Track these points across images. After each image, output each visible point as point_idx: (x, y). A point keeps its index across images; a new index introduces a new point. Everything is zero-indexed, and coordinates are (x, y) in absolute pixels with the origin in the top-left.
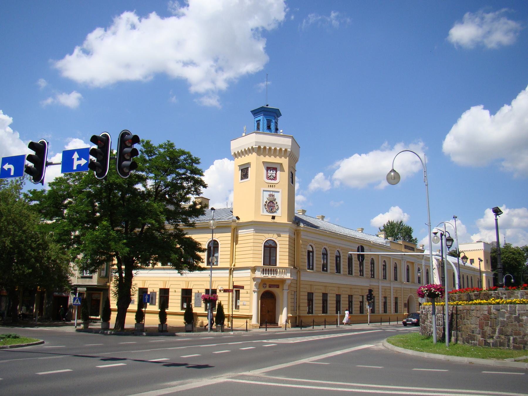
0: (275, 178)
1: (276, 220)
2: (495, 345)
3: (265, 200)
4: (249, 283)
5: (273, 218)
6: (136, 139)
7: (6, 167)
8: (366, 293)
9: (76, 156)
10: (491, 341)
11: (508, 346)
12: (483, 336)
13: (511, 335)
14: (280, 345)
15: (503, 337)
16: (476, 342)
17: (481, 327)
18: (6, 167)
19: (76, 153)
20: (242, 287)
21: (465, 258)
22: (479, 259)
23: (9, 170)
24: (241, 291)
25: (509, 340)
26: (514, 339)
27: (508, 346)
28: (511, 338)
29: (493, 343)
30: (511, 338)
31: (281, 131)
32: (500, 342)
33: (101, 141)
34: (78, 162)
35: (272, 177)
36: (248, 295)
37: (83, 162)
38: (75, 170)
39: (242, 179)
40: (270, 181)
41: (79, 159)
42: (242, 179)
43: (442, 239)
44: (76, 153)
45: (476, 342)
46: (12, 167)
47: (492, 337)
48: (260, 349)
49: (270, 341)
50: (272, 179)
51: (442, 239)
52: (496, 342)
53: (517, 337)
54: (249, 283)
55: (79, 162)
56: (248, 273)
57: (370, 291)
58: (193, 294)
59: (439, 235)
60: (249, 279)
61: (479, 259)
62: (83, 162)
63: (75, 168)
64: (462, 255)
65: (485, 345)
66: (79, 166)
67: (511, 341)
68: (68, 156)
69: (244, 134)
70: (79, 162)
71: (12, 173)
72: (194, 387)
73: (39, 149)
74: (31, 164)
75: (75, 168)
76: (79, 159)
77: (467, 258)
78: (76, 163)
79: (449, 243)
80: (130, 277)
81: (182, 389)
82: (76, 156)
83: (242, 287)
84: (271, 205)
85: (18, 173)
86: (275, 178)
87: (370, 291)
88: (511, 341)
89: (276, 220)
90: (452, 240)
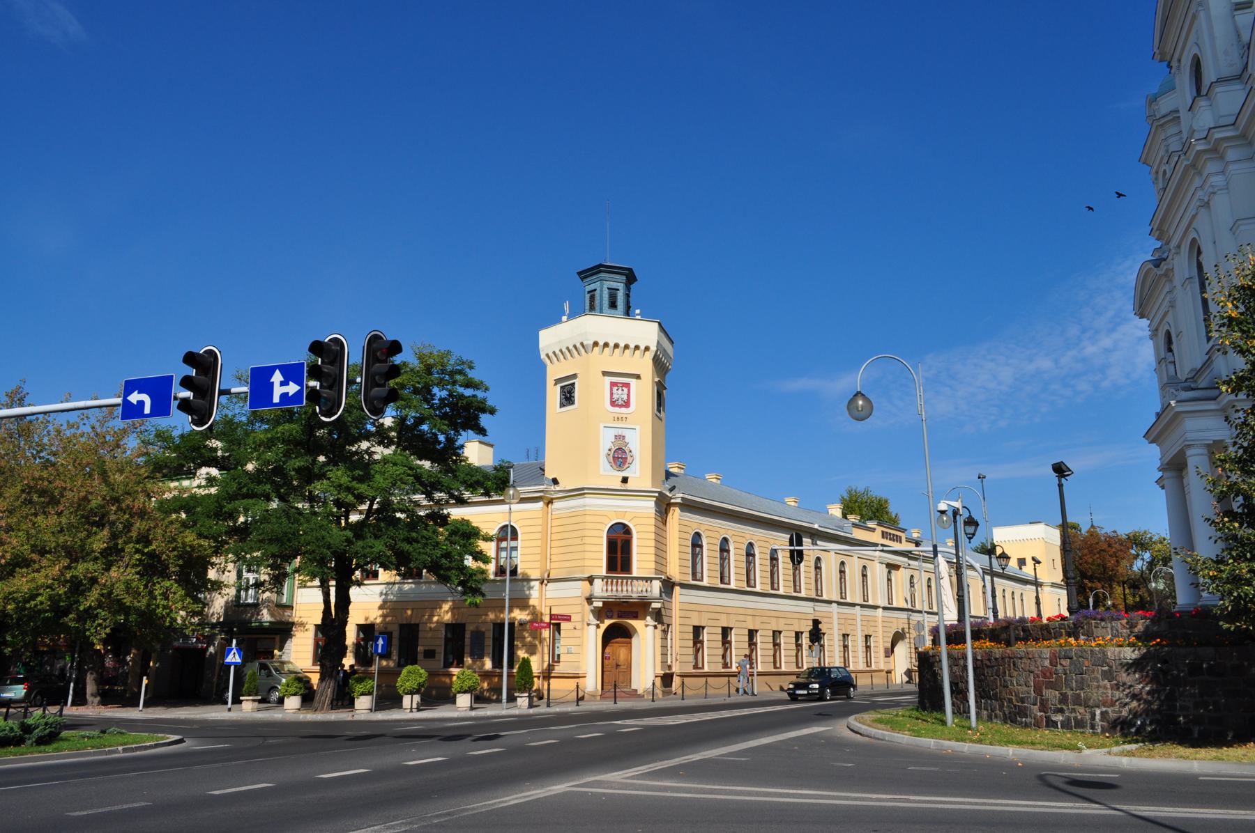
0: (627, 404)
1: (630, 486)
2: (1066, 725)
3: (609, 445)
4: (578, 609)
5: (625, 480)
6: (396, 347)
7: (134, 398)
8: (807, 627)
9: (277, 377)
10: (1058, 718)
11: (1093, 727)
12: (1043, 708)
13: (1098, 707)
14: (648, 729)
15: (1082, 710)
16: (1029, 720)
17: (1038, 690)
18: (134, 398)
19: (277, 373)
20: (568, 618)
21: (1004, 556)
22: (1033, 559)
23: (141, 403)
24: (564, 625)
25: (1093, 715)
26: (1102, 713)
27: (1093, 727)
28: (1098, 712)
29: (1062, 722)
30: (1098, 712)
31: (638, 311)
32: (1075, 718)
33: (329, 353)
34: (280, 388)
35: (620, 402)
36: (577, 633)
37: (292, 388)
38: (276, 404)
39: (562, 405)
40: (617, 409)
41: (282, 384)
42: (562, 405)
43: (955, 522)
44: (277, 373)
45: (1029, 720)
46: (146, 399)
47: (1061, 711)
48: (612, 736)
49: (629, 722)
50: (620, 406)
51: (955, 522)
52: (1069, 719)
53: (1109, 710)
54: (578, 609)
55: (285, 389)
56: (581, 589)
57: (816, 623)
58: (468, 635)
59: (950, 514)
60: (578, 601)
61: (1033, 559)
62: (292, 388)
63: (276, 399)
64: (999, 551)
65: (1047, 726)
66: (284, 396)
67: (1098, 717)
68: (261, 378)
69: (564, 318)
70: (285, 389)
71: (147, 410)
72: (1203, 752)
73: (203, 364)
74: (188, 394)
75: (276, 399)
76: (282, 384)
77: (1008, 558)
78: (278, 391)
79: (971, 529)
80: (344, 601)
81: (1212, 752)
82: (277, 377)
83: (568, 618)
84: (620, 457)
85: (161, 408)
86: (627, 404)
87: (816, 623)
88: (1098, 717)
89: (630, 486)
90: (977, 524)
